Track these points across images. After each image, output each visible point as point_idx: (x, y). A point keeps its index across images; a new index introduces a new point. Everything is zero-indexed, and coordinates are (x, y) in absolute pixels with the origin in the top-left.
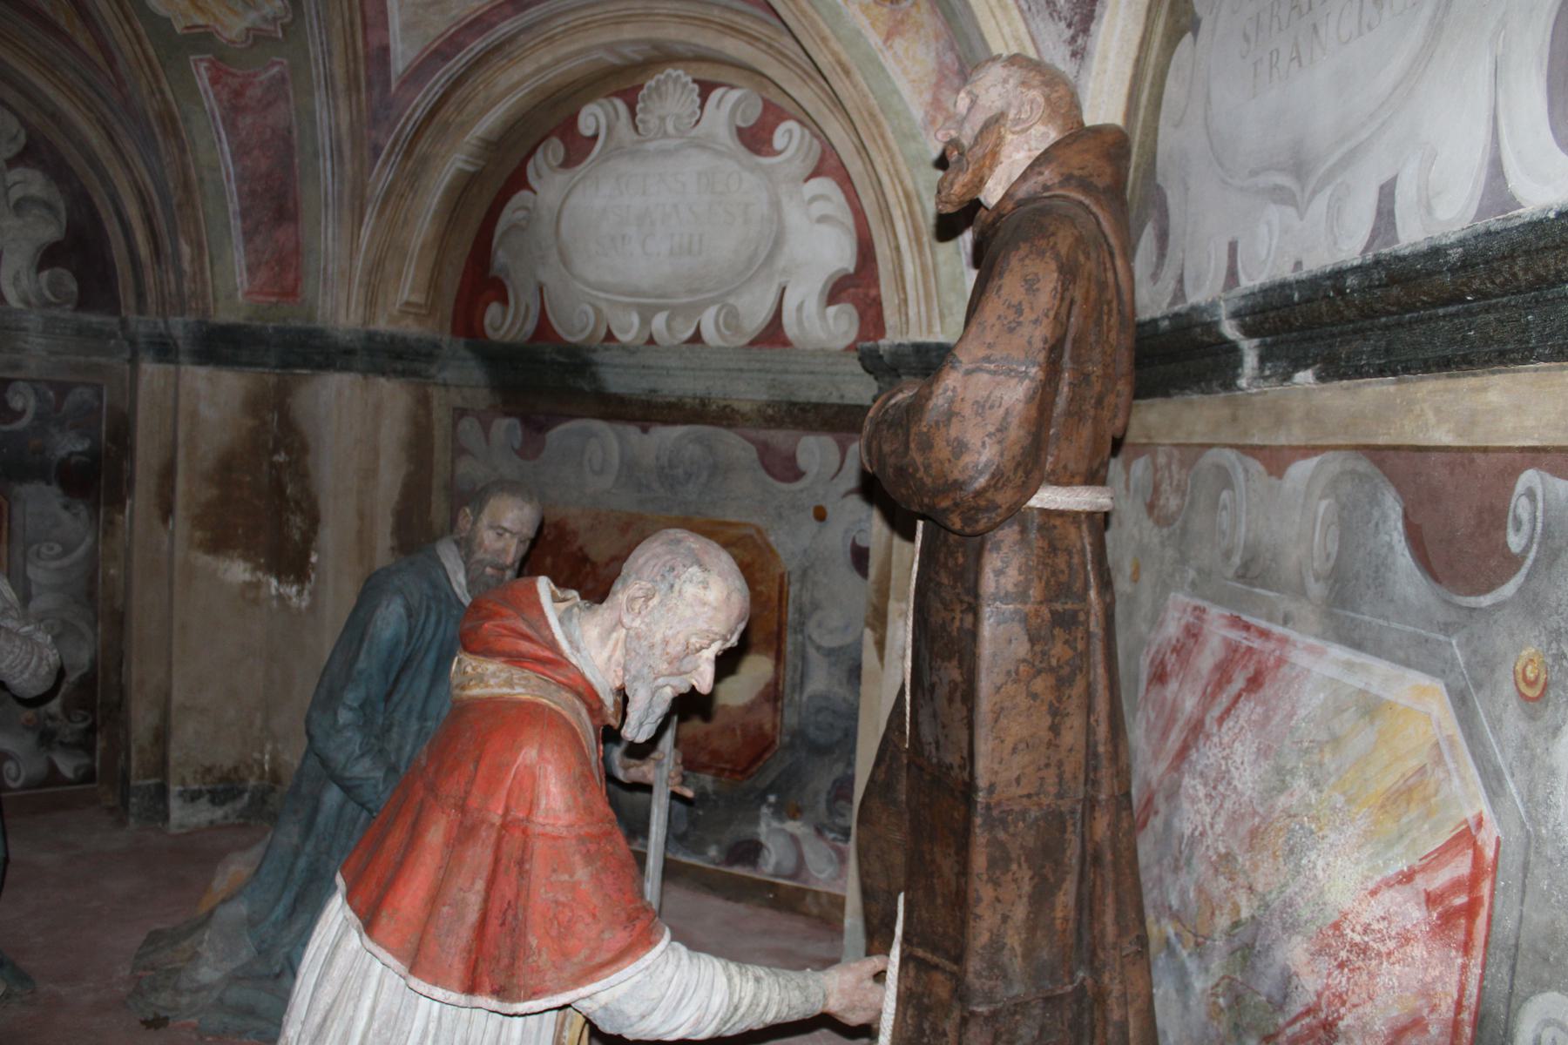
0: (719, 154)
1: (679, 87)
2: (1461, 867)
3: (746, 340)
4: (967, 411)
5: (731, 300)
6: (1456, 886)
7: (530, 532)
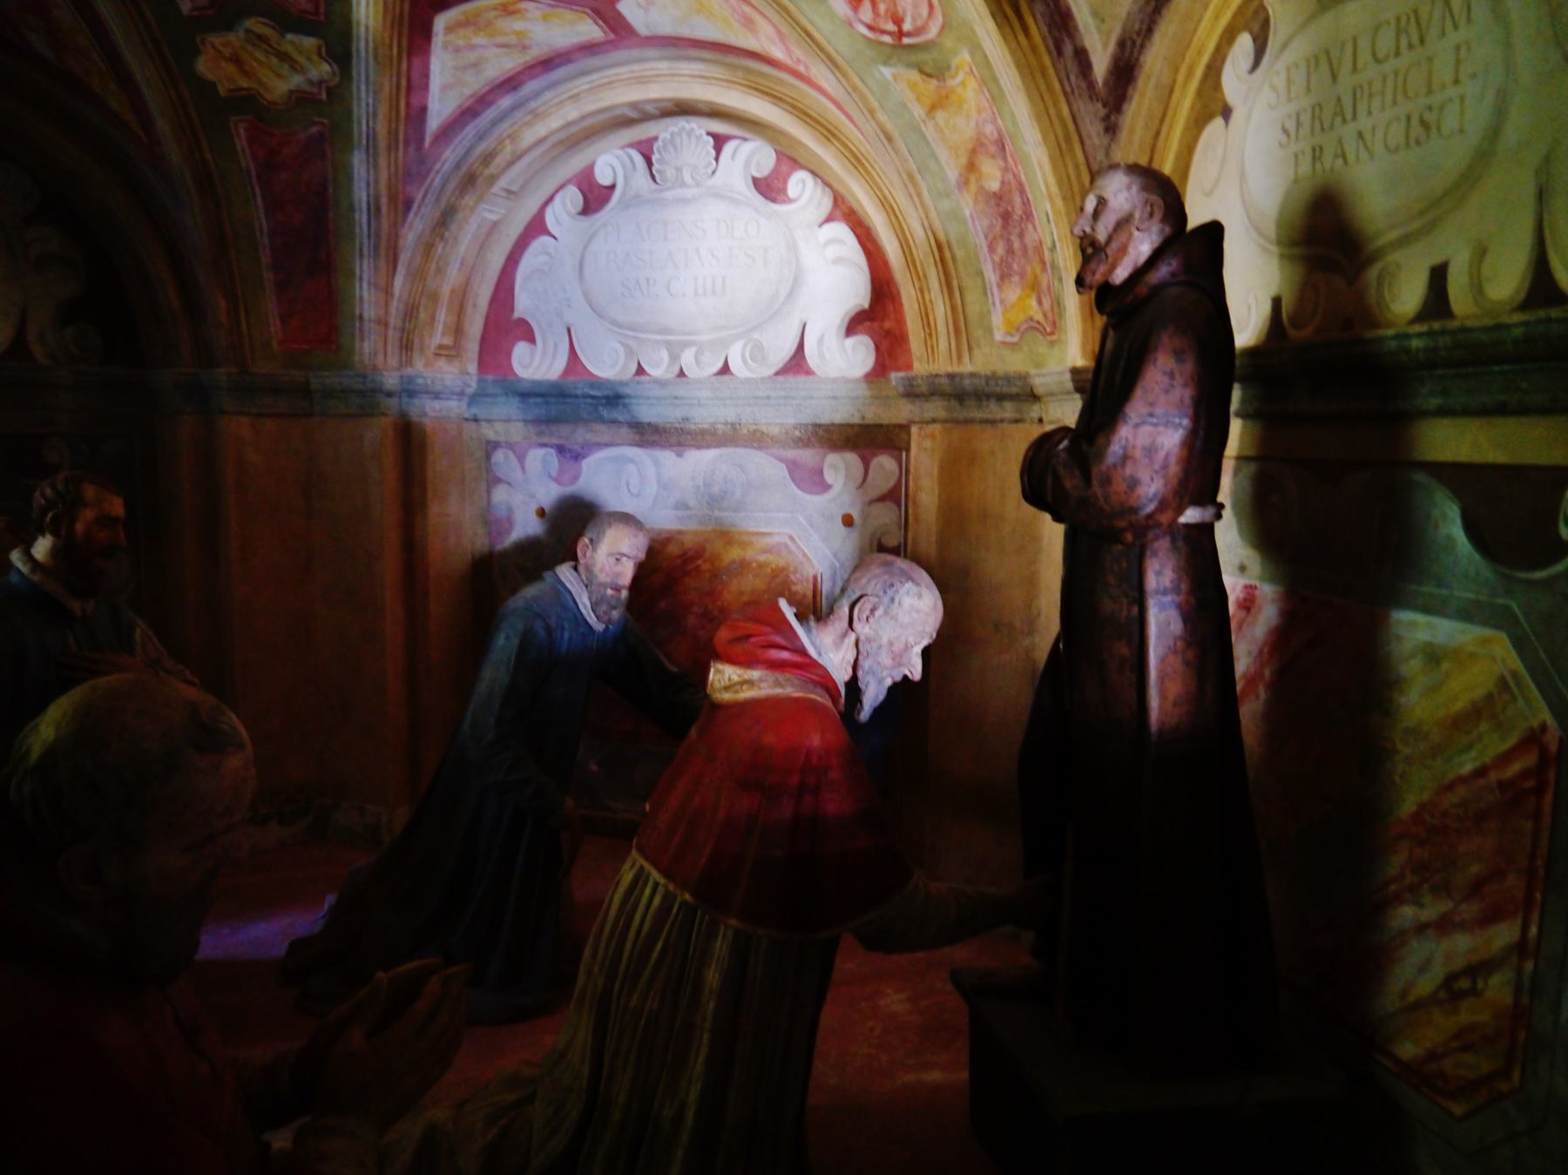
1: (693, 140)
2: (1529, 760)
3: (773, 371)
4: (1138, 454)
5: (756, 336)
6: (1525, 774)
7: (642, 556)
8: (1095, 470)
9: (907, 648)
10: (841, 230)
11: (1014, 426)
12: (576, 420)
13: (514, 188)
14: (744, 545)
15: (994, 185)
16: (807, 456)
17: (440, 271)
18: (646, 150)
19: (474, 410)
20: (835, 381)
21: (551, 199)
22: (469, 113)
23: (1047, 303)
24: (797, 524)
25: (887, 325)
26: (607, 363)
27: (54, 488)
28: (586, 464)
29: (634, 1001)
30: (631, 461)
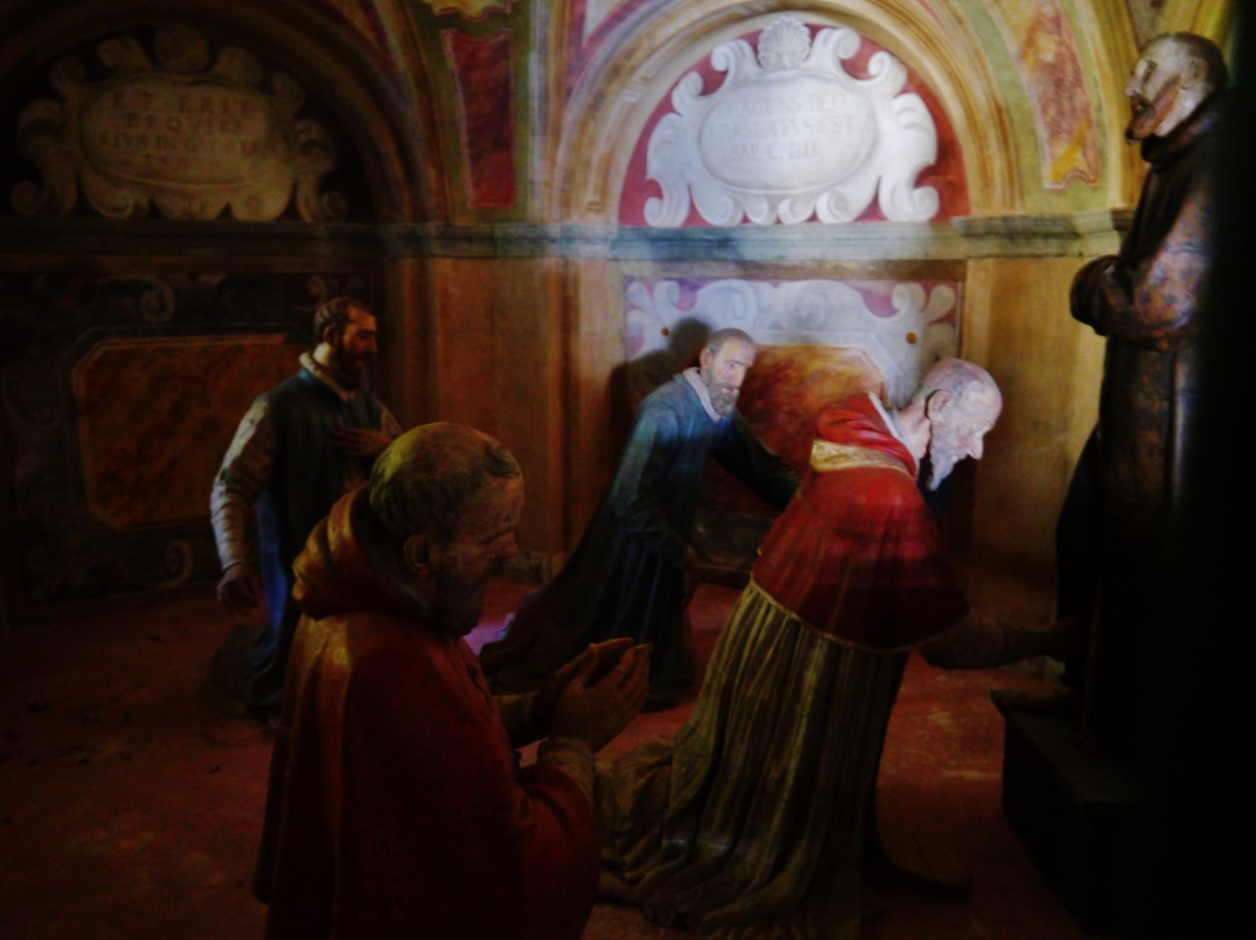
0: (827, 80)
3: (849, 218)
5: (840, 189)
7: (750, 363)
8: (1138, 290)
9: (972, 433)
10: (913, 101)
11: (1057, 260)
12: (694, 259)
13: (649, 76)
14: (825, 358)
15: (1049, 57)
16: (879, 286)
17: (592, 144)
18: (753, 40)
19: (616, 253)
20: (903, 225)
21: (676, 84)
22: (616, 18)
23: (1091, 154)
24: (869, 343)
25: (950, 177)
26: (718, 214)
27: (329, 309)
28: (703, 293)
29: (750, 693)
30: (737, 291)
